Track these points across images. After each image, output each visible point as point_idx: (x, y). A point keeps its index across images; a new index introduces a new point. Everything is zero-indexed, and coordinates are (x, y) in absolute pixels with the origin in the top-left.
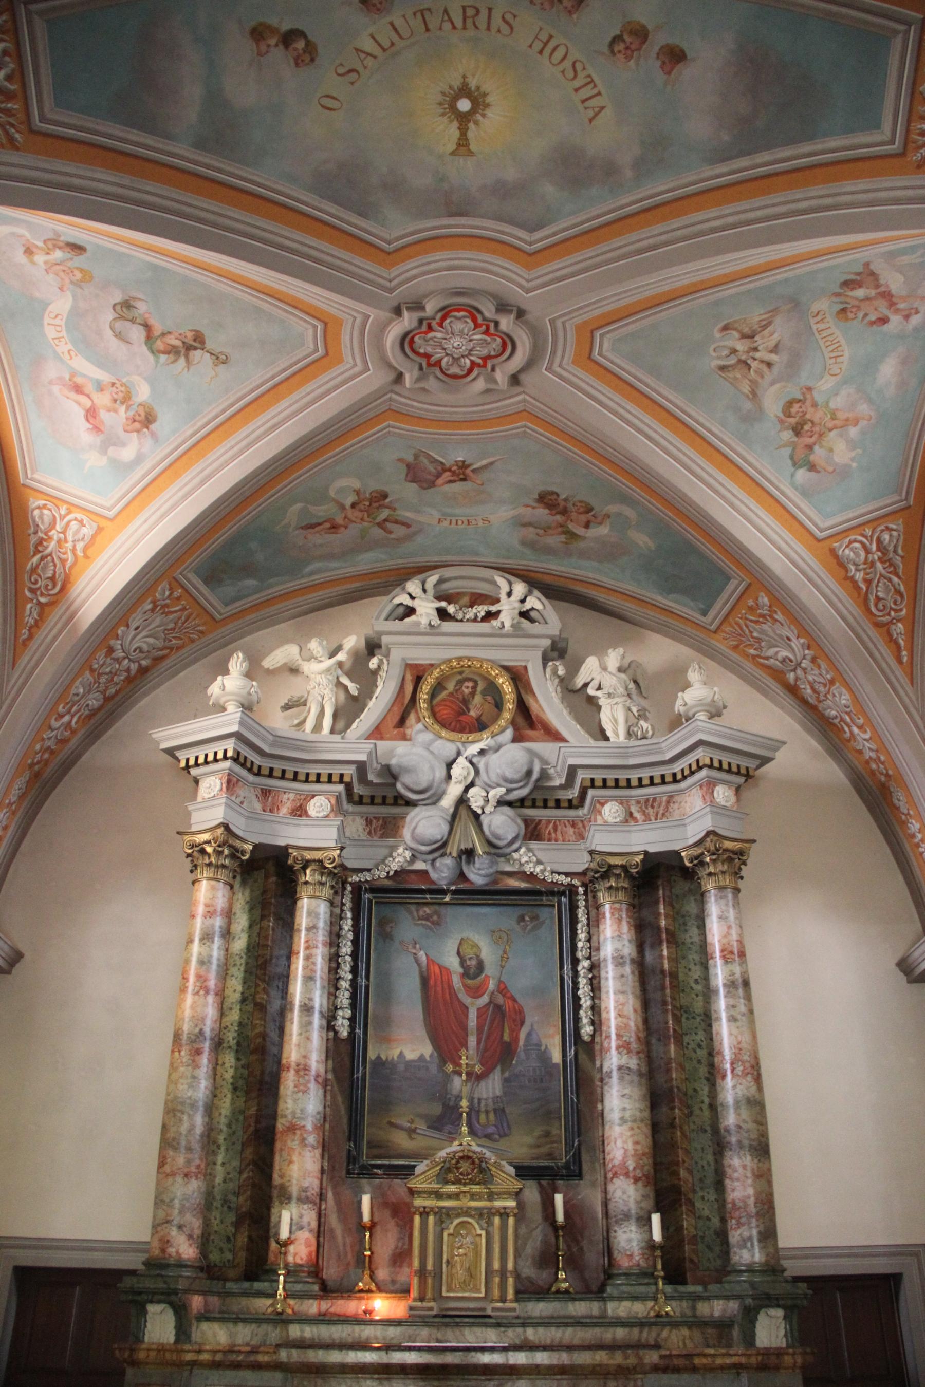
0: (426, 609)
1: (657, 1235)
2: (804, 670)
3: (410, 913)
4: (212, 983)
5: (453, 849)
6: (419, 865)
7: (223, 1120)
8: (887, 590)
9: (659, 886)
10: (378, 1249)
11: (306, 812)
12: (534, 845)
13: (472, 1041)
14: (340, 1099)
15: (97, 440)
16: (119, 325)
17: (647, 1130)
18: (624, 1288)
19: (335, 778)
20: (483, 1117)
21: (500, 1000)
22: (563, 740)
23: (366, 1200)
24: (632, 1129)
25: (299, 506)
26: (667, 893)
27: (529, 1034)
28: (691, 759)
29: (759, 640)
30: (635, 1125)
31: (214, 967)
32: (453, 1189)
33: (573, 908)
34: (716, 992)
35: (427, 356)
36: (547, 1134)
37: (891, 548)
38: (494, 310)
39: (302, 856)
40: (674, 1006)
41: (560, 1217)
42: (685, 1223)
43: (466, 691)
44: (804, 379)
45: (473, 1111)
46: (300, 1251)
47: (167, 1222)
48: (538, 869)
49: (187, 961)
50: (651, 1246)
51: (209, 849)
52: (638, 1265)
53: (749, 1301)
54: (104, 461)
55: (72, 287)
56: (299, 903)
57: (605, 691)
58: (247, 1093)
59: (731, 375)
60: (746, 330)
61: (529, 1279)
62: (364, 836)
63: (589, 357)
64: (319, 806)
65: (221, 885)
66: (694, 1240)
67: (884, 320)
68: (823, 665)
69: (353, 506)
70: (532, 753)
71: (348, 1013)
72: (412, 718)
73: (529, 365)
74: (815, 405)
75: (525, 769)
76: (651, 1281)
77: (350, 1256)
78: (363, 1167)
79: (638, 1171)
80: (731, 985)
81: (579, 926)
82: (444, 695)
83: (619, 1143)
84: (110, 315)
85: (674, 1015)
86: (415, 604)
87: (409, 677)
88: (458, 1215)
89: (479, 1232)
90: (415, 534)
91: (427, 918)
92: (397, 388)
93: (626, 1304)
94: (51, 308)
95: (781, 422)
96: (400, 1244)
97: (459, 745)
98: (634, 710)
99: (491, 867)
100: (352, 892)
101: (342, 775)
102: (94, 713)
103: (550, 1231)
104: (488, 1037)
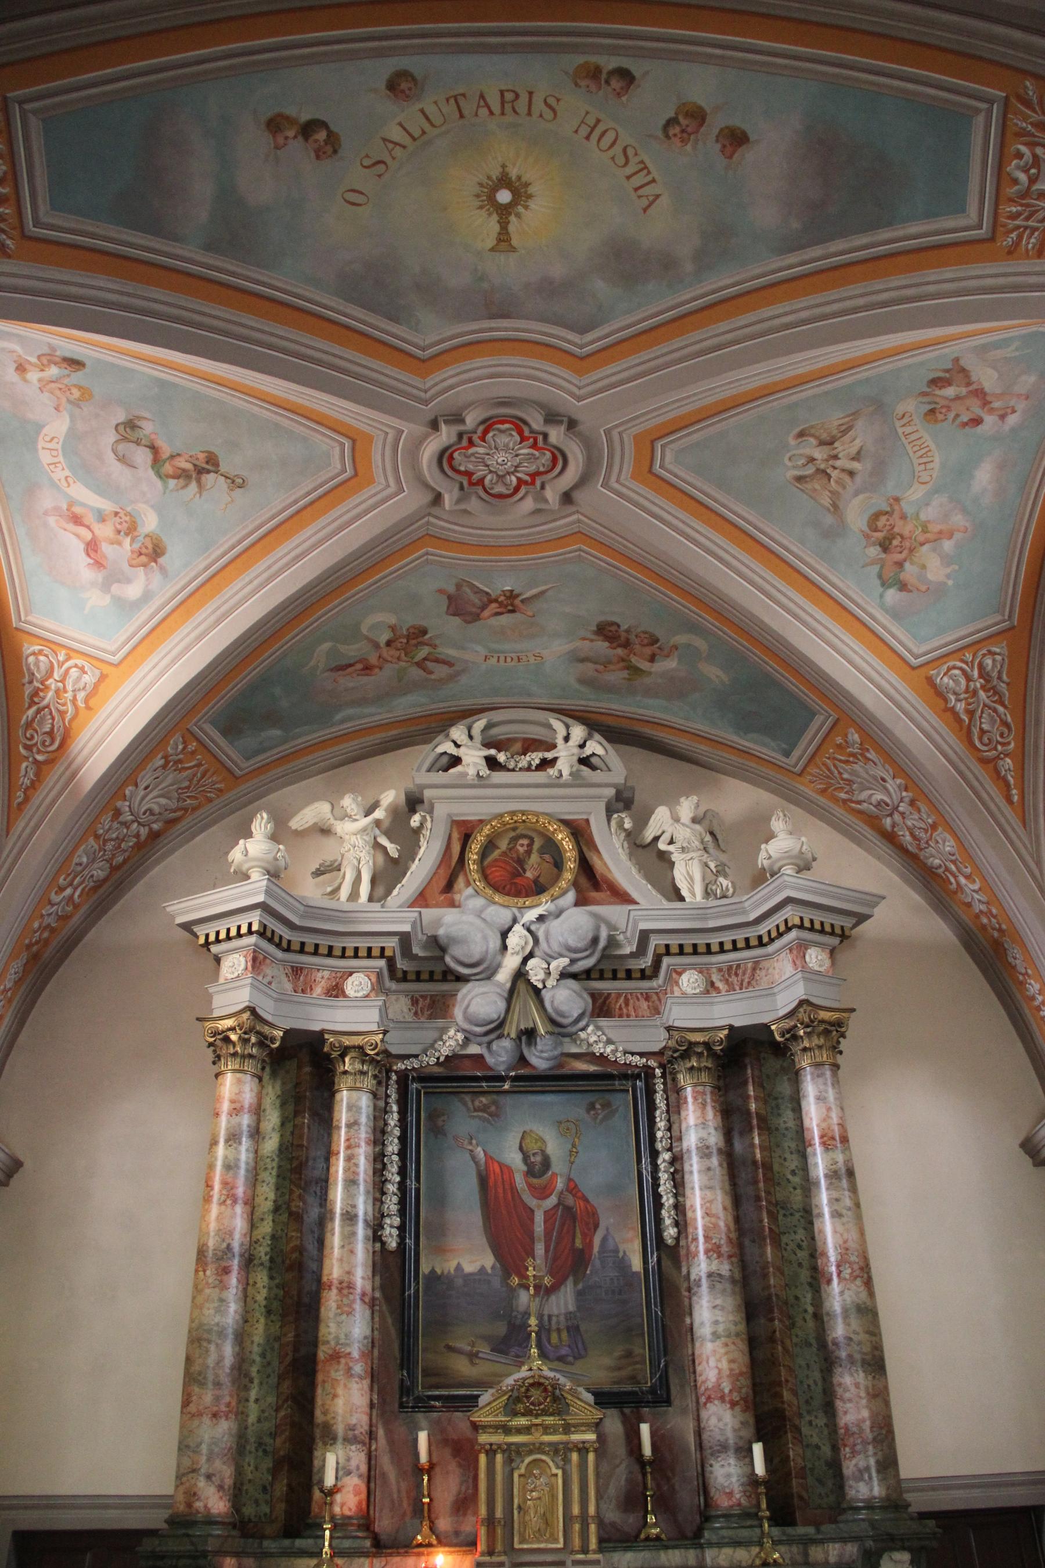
0: (473, 758)
1: (760, 1469)
2: (902, 814)
3: (465, 1104)
4: (240, 1191)
5: (512, 1029)
6: (474, 1049)
7: (256, 1349)
8: (993, 722)
9: (748, 1064)
10: (437, 1494)
11: (343, 992)
12: (603, 1022)
13: (540, 1249)
14: (389, 1321)
15: (99, 576)
16: (121, 447)
17: (743, 1346)
18: (724, 1532)
19: (376, 952)
20: (554, 1336)
21: (570, 1200)
22: (633, 902)
23: (423, 1437)
24: (727, 1345)
25: (326, 646)
26: (757, 1073)
27: (604, 1240)
28: (778, 919)
29: (850, 782)
30: (729, 1341)
31: (242, 1172)
32: (523, 1421)
33: (650, 1092)
34: (817, 1184)
35: (469, 474)
36: (629, 1354)
37: (995, 674)
38: (541, 420)
39: (340, 1042)
40: (769, 1202)
41: (647, 1450)
42: (791, 1453)
43: (521, 850)
44: (890, 488)
45: (544, 1330)
46: (348, 1500)
47: (194, 1471)
48: (609, 1049)
49: (211, 1167)
50: (753, 1481)
51: (234, 1037)
52: (739, 1505)
53: (869, 1544)
54: (107, 600)
55: (69, 406)
56: (338, 1096)
57: (678, 845)
58: (283, 1316)
59: (809, 486)
60: (824, 436)
61: (613, 1524)
62: (409, 1017)
63: (650, 471)
64: (357, 985)
65: (248, 1077)
66: (802, 1473)
67: (977, 421)
68: (924, 808)
69: (389, 644)
70: (596, 916)
71: (397, 1221)
72: (461, 882)
73: (583, 481)
74: (903, 517)
75: (590, 936)
76: (756, 1523)
77: (405, 1504)
78: (418, 1399)
79: (735, 1394)
80: (833, 1176)
81: (658, 1113)
82: (496, 854)
83: (712, 1363)
84: (111, 437)
85: (769, 1212)
86: (461, 752)
87: (456, 835)
88: (531, 1452)
89: (554, 1471)
90: (458, 674)
91: (484, 1109)
92: (435, 511)
93: (727, 1551)
94: (45, 430)
95: (867, 536)
96: (463, 1488)
97: (515, 910)
98: (712, 865)
99: (555, 1048)
100: (397, 1082)
101: (383, 949)
102: (100, 884)
103: (636, 1468)
104: (557, 1244)
